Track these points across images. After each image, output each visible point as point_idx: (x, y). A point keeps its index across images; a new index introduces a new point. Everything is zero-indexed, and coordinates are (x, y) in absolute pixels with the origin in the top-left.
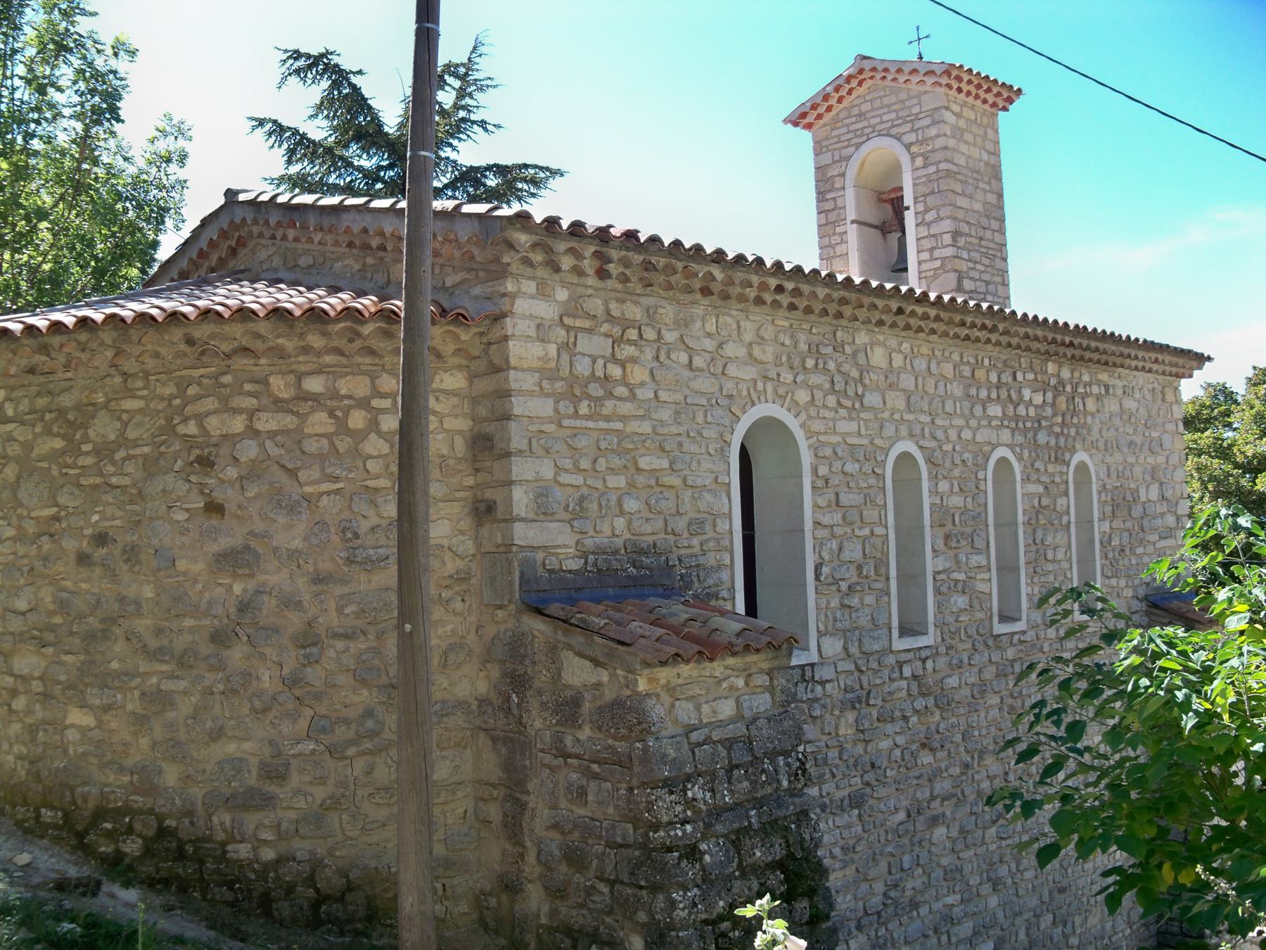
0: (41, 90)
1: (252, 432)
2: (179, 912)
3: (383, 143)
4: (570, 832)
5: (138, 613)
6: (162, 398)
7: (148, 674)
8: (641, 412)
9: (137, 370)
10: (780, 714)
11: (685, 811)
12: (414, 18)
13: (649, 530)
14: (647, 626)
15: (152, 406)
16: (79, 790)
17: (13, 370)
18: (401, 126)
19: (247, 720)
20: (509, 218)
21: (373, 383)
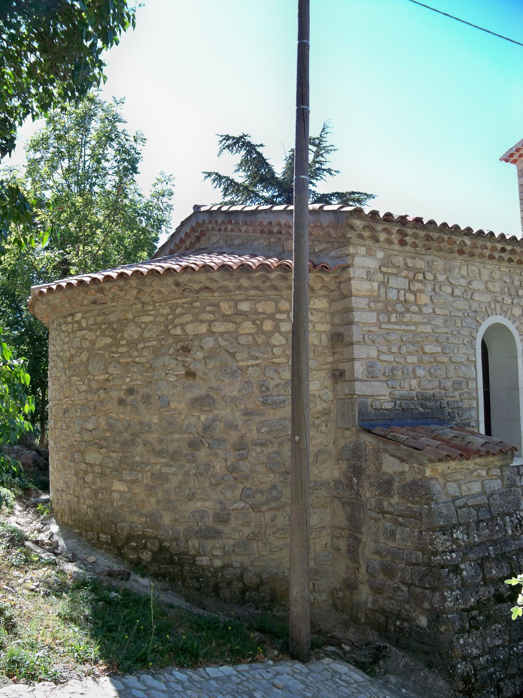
0: (99, 162)
1: (211, 333)
2: (170, 592)
3: (275, 183)
4: (385, 556)
5: (150, 431)
6: (162, 315)
7: (155, 464)
8: (425, 320)
9: (149, 301)
10: (507, 492)
11: (452, 545)
12: (295, 103)
13: (431, 387)
14: (430, 440)
15: (157, 319)
16: (119, 525)
17: (85, 303)
18: (284, 173)
19: (208, 490)
20: (350, 212)
21: (276, 306)
